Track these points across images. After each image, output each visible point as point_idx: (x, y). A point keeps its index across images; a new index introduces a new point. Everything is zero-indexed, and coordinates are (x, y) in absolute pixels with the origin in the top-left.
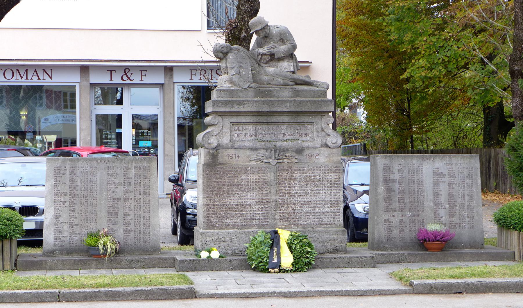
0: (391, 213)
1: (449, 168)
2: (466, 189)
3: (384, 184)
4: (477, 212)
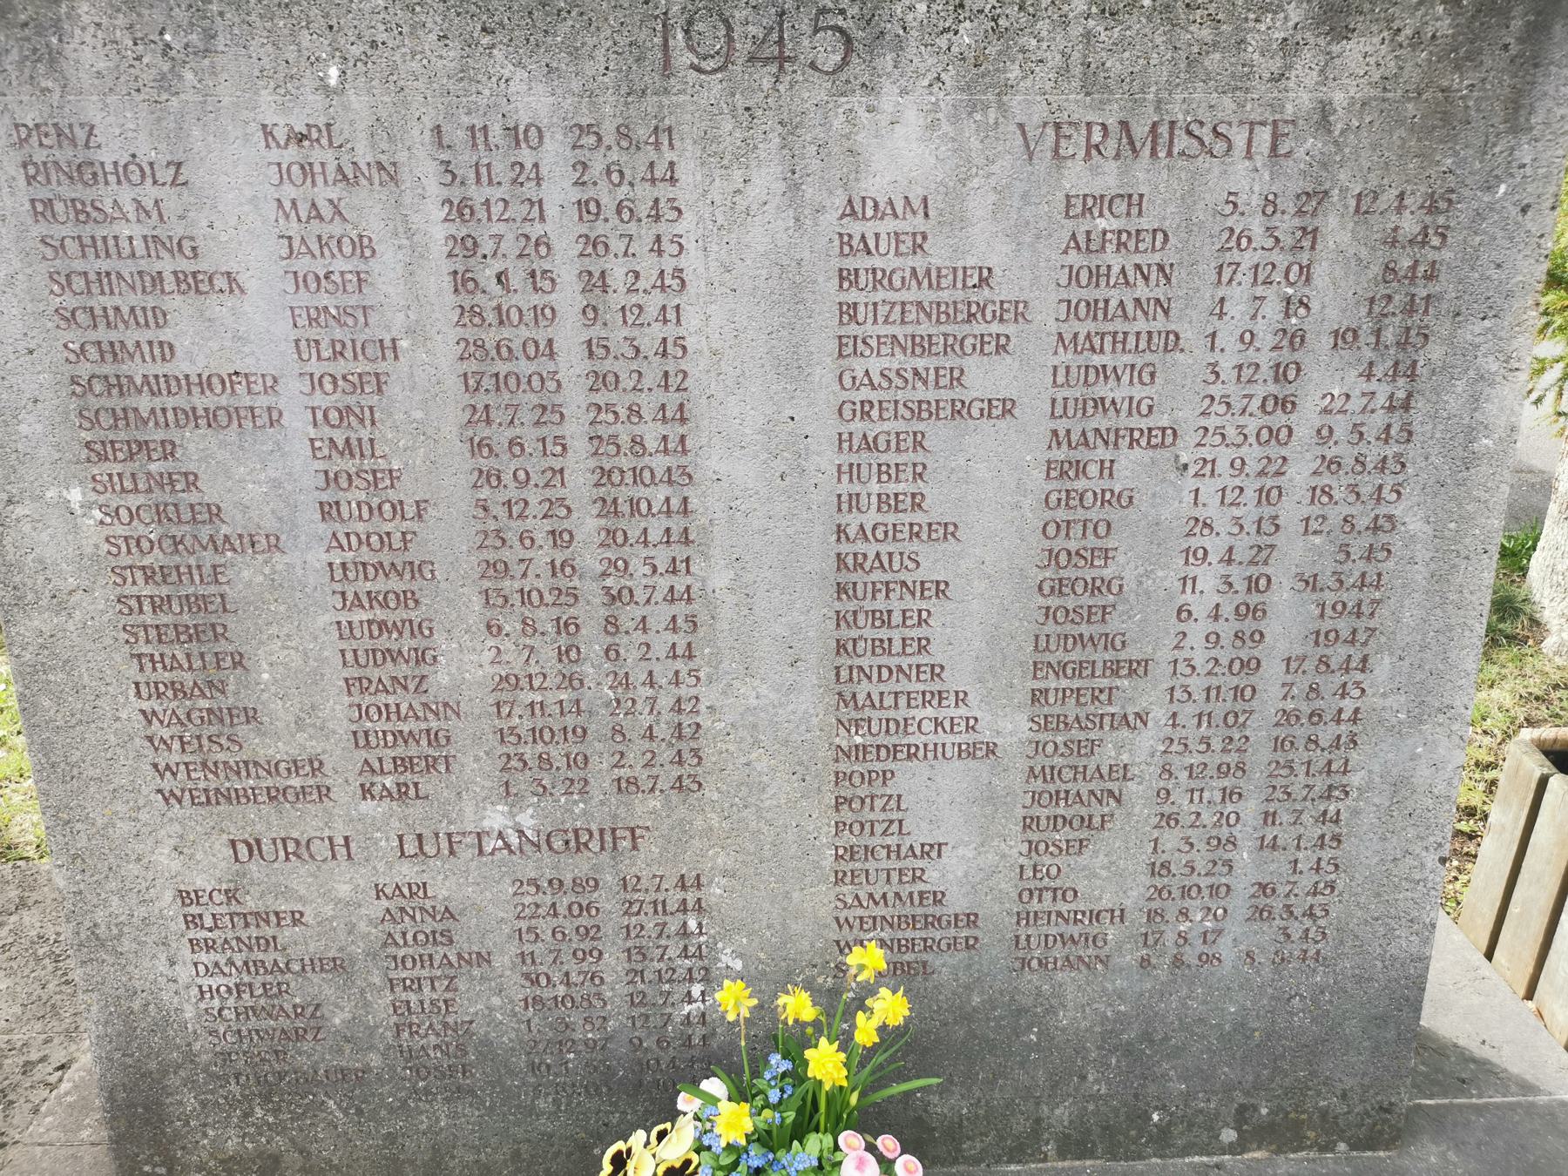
0: (262, 821)
1: (1094, 204)
2: (1291, 511)
3: (99, 452)
4: (1399, 785)
